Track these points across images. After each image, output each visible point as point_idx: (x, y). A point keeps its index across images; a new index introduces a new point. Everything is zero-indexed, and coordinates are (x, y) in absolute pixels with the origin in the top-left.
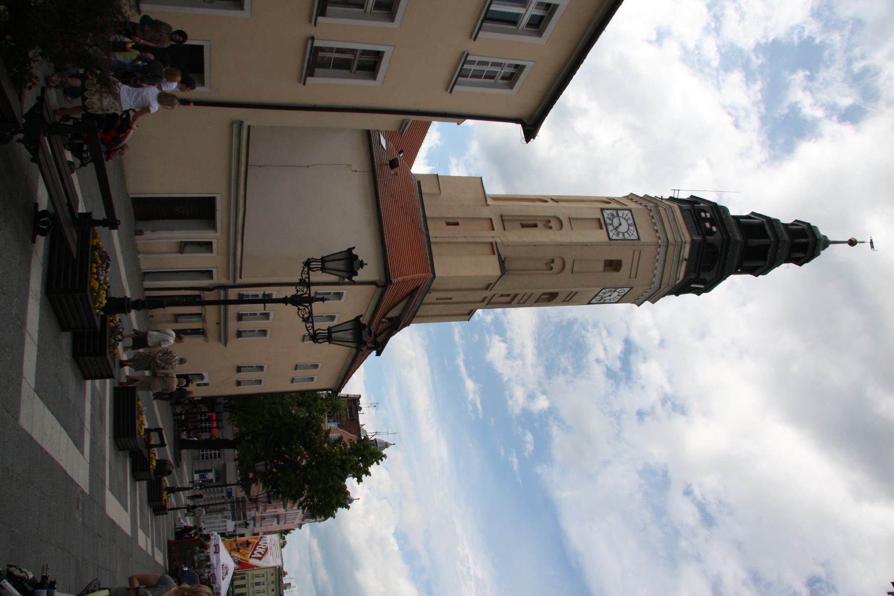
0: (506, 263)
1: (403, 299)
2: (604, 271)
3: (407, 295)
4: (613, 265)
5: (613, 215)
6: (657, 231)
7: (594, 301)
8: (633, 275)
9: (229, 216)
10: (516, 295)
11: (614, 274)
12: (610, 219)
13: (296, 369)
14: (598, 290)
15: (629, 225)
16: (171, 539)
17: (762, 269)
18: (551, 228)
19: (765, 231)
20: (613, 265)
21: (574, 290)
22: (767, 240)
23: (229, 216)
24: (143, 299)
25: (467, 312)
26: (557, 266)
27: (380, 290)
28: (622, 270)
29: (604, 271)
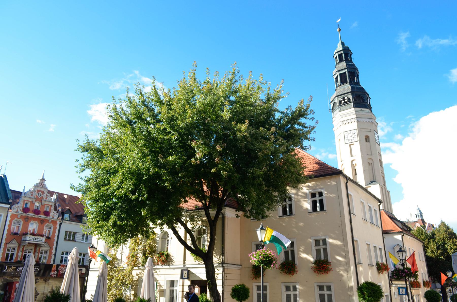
2: (369, 142)
4: (367, 139)
11: (370, 138)
20: (367, 139)
26: (371, 162)
29: (369, 142)
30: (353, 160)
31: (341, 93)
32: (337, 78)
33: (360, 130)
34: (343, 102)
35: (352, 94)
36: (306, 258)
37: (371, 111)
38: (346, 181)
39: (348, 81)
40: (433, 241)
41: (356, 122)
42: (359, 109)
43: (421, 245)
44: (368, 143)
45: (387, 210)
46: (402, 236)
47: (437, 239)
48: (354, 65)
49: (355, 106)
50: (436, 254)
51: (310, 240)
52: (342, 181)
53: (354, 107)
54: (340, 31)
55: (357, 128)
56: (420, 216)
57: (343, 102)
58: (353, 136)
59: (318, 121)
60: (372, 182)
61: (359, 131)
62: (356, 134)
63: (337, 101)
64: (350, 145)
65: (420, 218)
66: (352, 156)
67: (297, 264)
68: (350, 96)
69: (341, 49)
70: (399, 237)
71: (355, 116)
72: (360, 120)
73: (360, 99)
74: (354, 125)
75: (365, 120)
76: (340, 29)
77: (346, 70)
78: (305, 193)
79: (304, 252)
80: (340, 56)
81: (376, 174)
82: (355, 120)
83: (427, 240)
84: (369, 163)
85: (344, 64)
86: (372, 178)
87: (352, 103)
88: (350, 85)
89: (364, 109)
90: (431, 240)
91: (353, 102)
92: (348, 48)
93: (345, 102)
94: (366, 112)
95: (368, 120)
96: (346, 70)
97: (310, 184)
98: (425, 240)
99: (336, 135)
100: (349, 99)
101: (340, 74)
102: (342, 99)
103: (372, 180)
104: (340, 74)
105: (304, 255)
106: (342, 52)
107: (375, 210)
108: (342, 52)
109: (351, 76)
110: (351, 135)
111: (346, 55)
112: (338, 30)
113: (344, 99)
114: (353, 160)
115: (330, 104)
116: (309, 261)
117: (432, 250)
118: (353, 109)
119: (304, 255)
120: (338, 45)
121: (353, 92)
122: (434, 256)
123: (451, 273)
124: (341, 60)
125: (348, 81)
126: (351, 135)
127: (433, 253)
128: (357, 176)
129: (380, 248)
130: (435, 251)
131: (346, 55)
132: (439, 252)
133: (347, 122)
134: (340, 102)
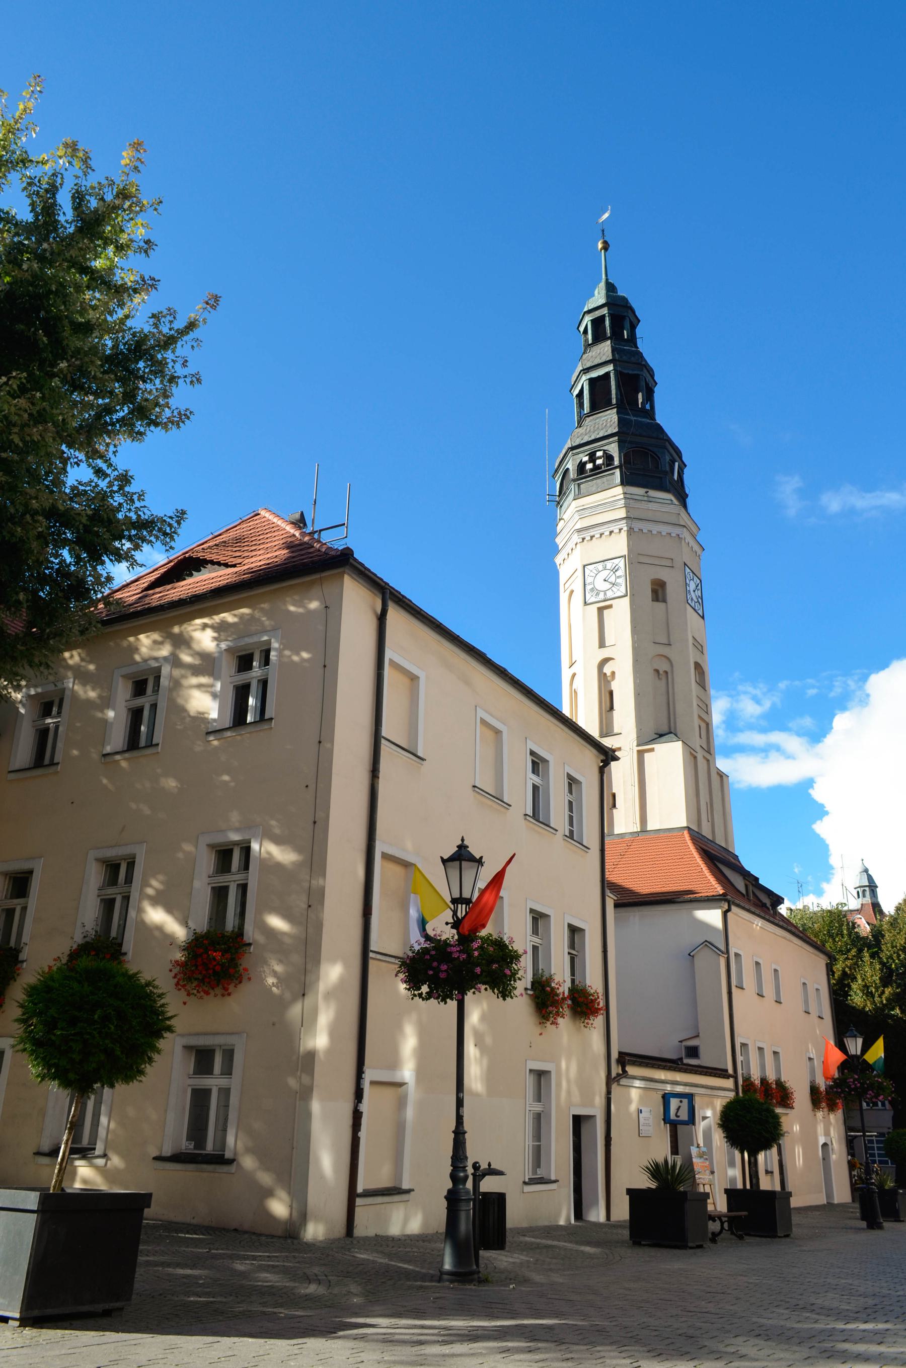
0: (661, 733)
1: (715, 865)
2: (664, 601)
3: (715, 865)
4: (659, 591)
5: (592, 590)
7: (700, 612)
10: (700, 717)
11: (669, 589)
12: (597, 594)
13: (780, 1003)
14: (689, 609)
15: (605, 569)
17: (649, 378)
18: (613, 673)
19: (599, 378)
20: (659, 591)
21: (691, 641)
22: (612, 375)
24: (892, 1113)
25: (718, 778)
26: (663, 666)
27: (733, 908)
28: (665, 580)
29: (664, 601)
30: (606, 661)
31: (586, 439)
32: (580, 395)
33: (636, 560)
34: (589, 466)
35: (619, 442)
36: (160, 928)
37: (685, 506)
38: (379, 609)
39: (614, 401)
40: (872, 956)
41: (624, 534)
42: (639, 491)
43: (821, 961)
44: (661, 605)
45: (706, 832)
46: (725, 914)
47: (886, 951)
48: (640, 355)
49: (623, 483)
50: (877, 999)
51: (188, 847)
52: (355, 604)
53: (623, 483)
54: (606, 247)
55: (625, 552)
56: (868, 893)
57: (589, 466)
58: (612, 579)
59: (216, 298)
60: (661, 736)
61: (631, 563)
62: (621, 573)
63: (571, 465)
64: (601, 610)
65: (868, 900)
66: (602, 644)
67: (130, 954)
68: (613, 449)
69: (602, 301)
70: (712, 917)
71: (622, 513)
72: (637, 525)
73: (649, 462)
74: (619, 544)
75: (656, 528)
76: (605, 243)
77: (610, 368)
78: (205, 656)
79: (156, 901)
80: (598, 323)
81: (680, 707)
82: (623, 525)
83: (854, 952)
84: (657, 671)
85: (605, 350)
86: (665, 721)
87: (618, 472)
88: (618, 413)
89: (652, 493)
90: (866, 955)
91: (620, 467)
92: (624, 299)
93: (596, 467)
94: (661, 502)
95: (665, 529)
96: (610, 368)
97: (228, 617)
98: (849, 951)
99: (563, 578)
100: (609, 458)
101: (592, 381)
102: (586, 459)
103: (665, 729)
104: (592, 381)
105: (156, 916)
106: (605, 311)
107: (572, 782)
108: (605, 311)
109: (627, 387)
110: (604, 574)
111: (618, 321)
112: (600, 246)
113: (592, 457)
114: (606, 661)
115: (554, 477)
116: (169, 939)
117: (866, 987)
118: (619, 490)
119: (156, 916)
120: (596, 292)
121: (623, 435)
122: (869, 1007)
123: (860, 1041)
124: (599, 337)
125: (614, 401)
126: (604, 574)
127: (872, 995)
128: (615, 713)
129: (574, 931)
130: (877, 988)
131: (618, 321)
132: (888, 991)
133: (596, 532)
134: (581, 466)
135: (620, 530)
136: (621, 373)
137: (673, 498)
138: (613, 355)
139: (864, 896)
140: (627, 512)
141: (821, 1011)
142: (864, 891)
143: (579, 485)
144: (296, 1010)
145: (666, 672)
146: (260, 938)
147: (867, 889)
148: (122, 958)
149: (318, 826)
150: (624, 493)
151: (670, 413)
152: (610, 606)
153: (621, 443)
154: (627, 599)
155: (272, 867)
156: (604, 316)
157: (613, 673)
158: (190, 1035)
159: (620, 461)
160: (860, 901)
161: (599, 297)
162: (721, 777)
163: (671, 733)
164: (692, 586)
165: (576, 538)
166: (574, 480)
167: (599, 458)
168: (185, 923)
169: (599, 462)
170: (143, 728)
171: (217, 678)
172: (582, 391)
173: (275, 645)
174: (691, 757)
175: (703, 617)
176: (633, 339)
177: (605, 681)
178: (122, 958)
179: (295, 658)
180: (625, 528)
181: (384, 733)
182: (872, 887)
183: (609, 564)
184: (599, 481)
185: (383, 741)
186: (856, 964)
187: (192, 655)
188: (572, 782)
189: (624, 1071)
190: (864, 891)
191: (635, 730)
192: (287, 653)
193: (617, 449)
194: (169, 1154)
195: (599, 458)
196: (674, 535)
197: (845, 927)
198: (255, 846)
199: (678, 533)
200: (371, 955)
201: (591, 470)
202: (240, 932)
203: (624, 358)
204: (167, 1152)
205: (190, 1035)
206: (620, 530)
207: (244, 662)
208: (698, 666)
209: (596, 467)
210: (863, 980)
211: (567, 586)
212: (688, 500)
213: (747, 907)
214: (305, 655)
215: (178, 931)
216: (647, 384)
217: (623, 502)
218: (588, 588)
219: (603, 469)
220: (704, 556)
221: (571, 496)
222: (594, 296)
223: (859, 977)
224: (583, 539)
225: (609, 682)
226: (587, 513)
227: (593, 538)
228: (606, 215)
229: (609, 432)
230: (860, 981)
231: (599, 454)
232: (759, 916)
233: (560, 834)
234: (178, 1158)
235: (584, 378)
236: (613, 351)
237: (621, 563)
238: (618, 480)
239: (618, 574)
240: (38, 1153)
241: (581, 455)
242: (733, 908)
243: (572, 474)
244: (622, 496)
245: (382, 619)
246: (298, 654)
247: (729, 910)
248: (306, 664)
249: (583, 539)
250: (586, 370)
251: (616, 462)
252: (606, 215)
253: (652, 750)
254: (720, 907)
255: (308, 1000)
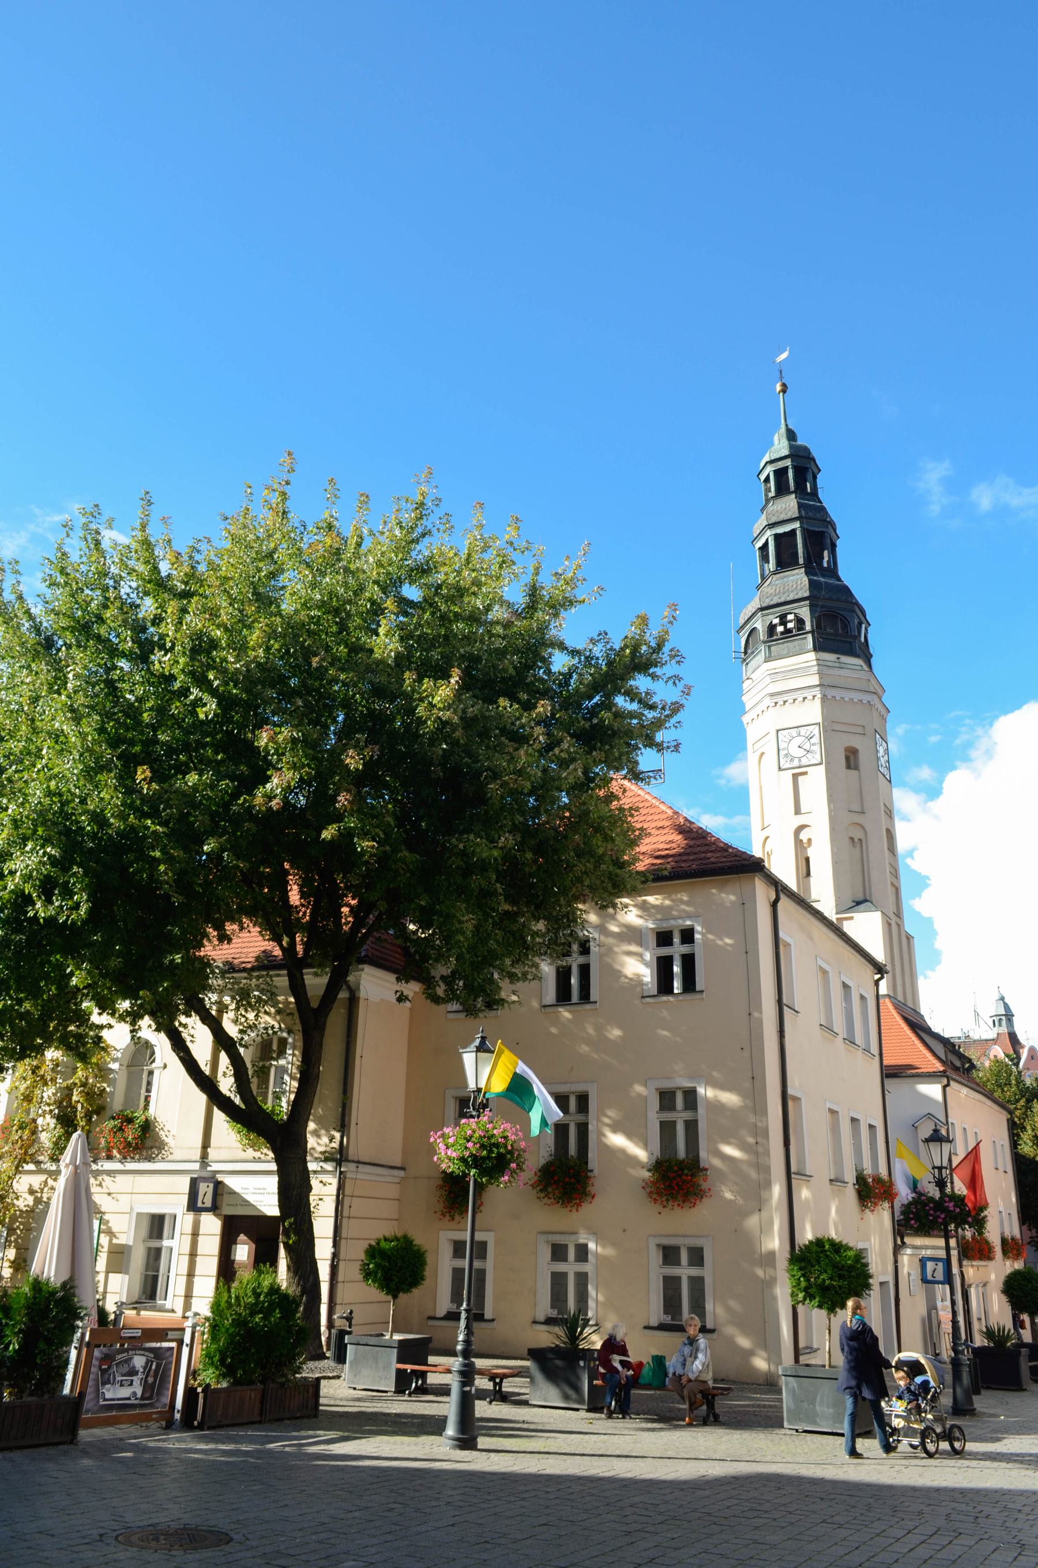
2: (857, 768)
4: (852, 759)
5: (786, 755)
6: (804, 699)
8: (860, 730)
9: (526, 1436)
15: (799, 735)
16: (1007, 1234)
18: (810, 840)
20: (852, 759)
21: (882, 808)
22: (798, 533)
23: (526, 1436)
26: (858, 834)
29: (857, 768)
33: (830, 727)
35: (811, 606)
36: (623, 1151)
37: (870, 666)
38: (773, 897)
39: (801, 561)
41: (818, 702)
42: (831, 657)
44: (854, 773)
45: (900, 998)
46: (944, 1088)
49: (815, 649)
51: (639, 1088)
54: (784, 389)
55: (820, 720)
56: (1004, 1023)
57: (780, 629)
58: (807, 746)
60: (858, 903)
61: (825, 731)
62: (815, 740)
63: (760, 624)
64: (795, 776)
65: (1004, 1029)
66: (798, 811)
67: (596, 1172)
68: (805, 612)
69: (785, 452)
70: (933, 1090)
71: (815, 680)
72: (831, 692)
73: (837, 625)
74: (812, 711)
75: (848, 695)
76: (784, 385)
77: (796, 525)
79: (615, 1129)
80: (781, 474)
81: (875, 876)
82: (817, 692)
83: (1022, 1102)
84: (852, 839)
87: (810, 637)
88: (807, 573)
89: (845, 659)
91: (812, 632)
93: (788, 631)
95: (856, 696)
96: (796, 525)
98: (1018, 1101)
100: (800, 622)
101: (777, 537)
102: (776, 621)
103: (860, 897)
104: (777, 537)
105: (617, 1140)
107: (862, 997)
109: (809, 544)
110: (799, 740)
112: (778, 388)
113: (783, 621)
116: (633, 1160)
118: (812, 656)
119: (617, 1140)
120: (776, 437)
121: (814, 599)
124: (782, 490)
125: (801, 561)
126: (799, 740)
129: (871, 1127)
131: (799, 473)
133: (790, 698)
134: (772, 628)
135: (814, 697)
136: (808, 530)
137: (862, 663)
138: (799, 512)
139: (1000, 1025)
140: (821, 678)
141: (1005, 1166)
142: (1000, 1020)
143: (769, 647)
144: (753, 1222)
145: (860, 840)
146: (716, 1162)
147: (1003, 1018)
148: (589, 1174)
149: (757, 1079)
150: (818, 660)
151: (853, 569)
152: (805, 773)
153: (812, 607)
154: (822, 768)
155: (717, 1107)
156: (787, 467)
157: (810, 840)
158: (661, 1236)
159: (812, 626)
160: (996, 1030)
161: (780, 447)
162: (908, 939)
163: (866, 901)
164: (881, 750)
165: (768, 701)
166: (764, 642)
167: (791, 621)
168: (646, 1146)
169: (790, 625)
170: (573, 981)
171: (647, 949)
172: (766, 544)
173: (698, 928)
174: (888, 925)
175: (890, 781)
176: (814, 494)
177: (801, 847)
178: (589, 1174)
179: (720, 942)
180: (819, 696)
181: (785, 1001)
182: (1009, 1016)
183: (803, 731)
184: (789, 644)
185: (785, 1008)
186: (1025, 1113)
187: (618, 926)
188: (862, 997)
189: (903, 1243)
190: (1000, 1020)
191: (833, 898)
192: (710, 936)
193: (808, 613)
194: (656, 1325)
195: (791, 621)
196: (865, 702)
197: (1013, 1077)
198: (701, 1090)
199: (870, 699)
200: (793, 1176)
201: (782, 633)
202: (696, 1159)
203: (811, 514)
204: (654, 1322)
205: (661, 1236)
206: (814, 697)
207: (664, 938)
208: (888, 830)
209: (788, 631)
210: (1033, 1130)
211: (756, 746)
212: (873, 660)
213: (960, 1079)
214: (728, 941)
215: (641, 1154)
216: (831, 540)
217: (816, 668)
218: (782, 753)
219: (794, 633)
220: (889, 717)
221: (761, 657)
222: (772, 444)
223: (1028, 1127)
224: (776, 703)
225: (805, 849)
226: (779, 677)
227: (782, 698)
228: (784, 356)
229: (800, 596)
230: (1030, 1132)
231: (790, 617)
232: (963, 1084)
233: (840, 1038)
234: (662, 1327)
235: (769, 533)
236: (799, 508)
237: (815, 730)
238: (811, 646)
239: (812, 741)
240: (535, 1322)
241: (771, 617)
242: (952, 1083)
243: (762, 634)
244: (815, 663)
245: (774, 905)
246: (721, 939)
247: (948, 1085)
248: (729, 948)
249: (776, 703)
250: (772, 526)
251: (808, 627)
252: (784, 356)
253: (852, 918)
254: (940, 1083)
255: (764, 1214)
